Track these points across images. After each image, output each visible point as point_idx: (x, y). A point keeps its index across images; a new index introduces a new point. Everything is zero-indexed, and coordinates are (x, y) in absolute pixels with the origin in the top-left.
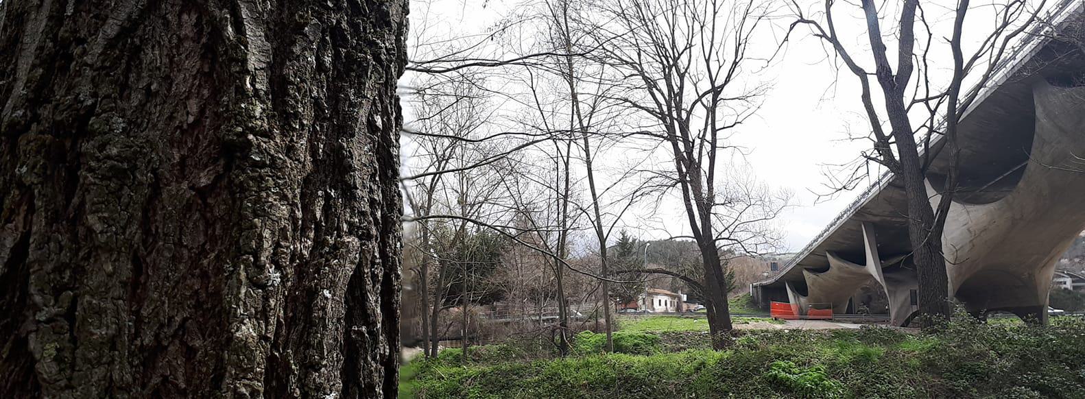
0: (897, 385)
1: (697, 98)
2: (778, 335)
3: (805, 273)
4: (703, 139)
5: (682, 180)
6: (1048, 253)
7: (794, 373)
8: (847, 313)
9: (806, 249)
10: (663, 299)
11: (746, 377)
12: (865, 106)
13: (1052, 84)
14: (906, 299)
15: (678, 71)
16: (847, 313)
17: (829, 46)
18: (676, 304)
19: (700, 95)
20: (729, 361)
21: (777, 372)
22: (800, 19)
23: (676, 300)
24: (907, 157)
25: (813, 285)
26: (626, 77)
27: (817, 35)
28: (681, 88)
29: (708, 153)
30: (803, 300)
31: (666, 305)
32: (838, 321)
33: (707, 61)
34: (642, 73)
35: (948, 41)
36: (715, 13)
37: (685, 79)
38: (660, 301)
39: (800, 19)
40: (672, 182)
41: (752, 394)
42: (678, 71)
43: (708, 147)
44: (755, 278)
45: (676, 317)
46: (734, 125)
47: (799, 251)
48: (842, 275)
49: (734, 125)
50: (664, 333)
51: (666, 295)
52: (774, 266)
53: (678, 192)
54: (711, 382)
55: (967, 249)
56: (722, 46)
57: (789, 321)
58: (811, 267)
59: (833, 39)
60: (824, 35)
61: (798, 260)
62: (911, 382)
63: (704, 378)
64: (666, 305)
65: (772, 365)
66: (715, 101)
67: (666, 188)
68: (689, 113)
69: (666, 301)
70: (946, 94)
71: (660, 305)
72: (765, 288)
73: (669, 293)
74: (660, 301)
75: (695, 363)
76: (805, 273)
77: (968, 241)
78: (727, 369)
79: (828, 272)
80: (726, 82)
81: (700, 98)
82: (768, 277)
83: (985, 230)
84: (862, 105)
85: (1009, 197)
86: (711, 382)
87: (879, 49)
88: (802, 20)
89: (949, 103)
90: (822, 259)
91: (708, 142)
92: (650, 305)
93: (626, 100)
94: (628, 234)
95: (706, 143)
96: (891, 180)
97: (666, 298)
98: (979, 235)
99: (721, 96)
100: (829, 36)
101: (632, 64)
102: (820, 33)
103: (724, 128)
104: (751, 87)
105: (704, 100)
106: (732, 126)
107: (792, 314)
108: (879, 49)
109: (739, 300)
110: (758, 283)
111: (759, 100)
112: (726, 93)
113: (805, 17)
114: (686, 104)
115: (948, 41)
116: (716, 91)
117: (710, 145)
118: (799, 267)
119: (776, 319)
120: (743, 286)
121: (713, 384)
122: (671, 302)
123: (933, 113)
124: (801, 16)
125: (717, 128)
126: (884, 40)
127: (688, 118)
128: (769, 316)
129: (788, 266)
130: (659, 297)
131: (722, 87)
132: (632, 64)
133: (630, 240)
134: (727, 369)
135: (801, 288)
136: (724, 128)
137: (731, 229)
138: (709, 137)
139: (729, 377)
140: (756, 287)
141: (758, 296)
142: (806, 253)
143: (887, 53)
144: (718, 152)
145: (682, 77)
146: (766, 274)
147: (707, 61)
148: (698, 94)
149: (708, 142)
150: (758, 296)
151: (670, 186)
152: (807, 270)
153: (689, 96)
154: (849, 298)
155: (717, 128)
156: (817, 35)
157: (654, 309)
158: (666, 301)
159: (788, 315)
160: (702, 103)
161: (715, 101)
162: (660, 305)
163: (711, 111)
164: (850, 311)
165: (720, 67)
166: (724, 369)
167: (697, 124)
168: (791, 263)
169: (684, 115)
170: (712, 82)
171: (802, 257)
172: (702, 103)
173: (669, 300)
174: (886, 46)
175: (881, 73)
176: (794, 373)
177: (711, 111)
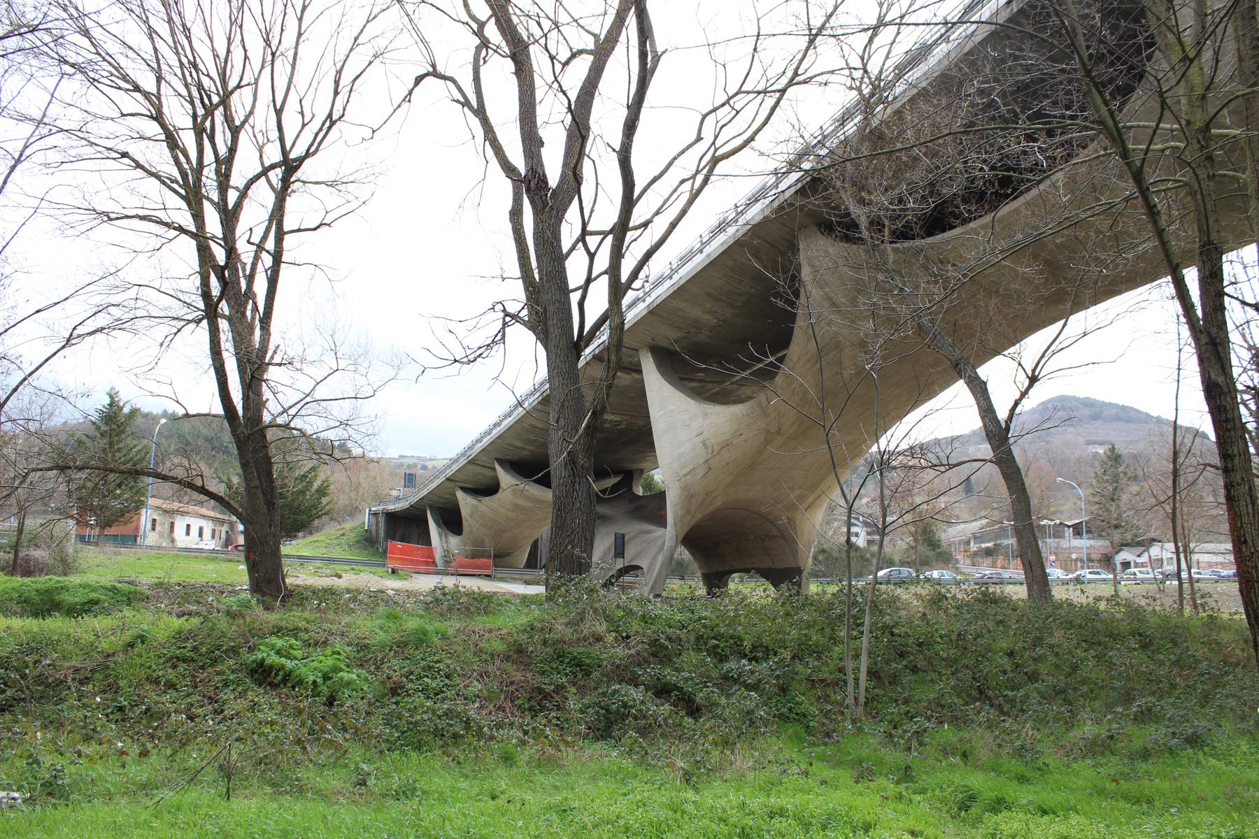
0: (457, 680)
1: (260, 169)
2: (377, 597)
3: (460, 495)
4: (260, 247)
5: (211, 313)
6: (812, 489)
7: (296, 658)
8: (525, 567)
9: (463, 454)
10: (196, 524)
11: (215, 661)
12: (513, 228)
13: (821, 233)
14: (609, 549)
15: (228, 119)
16: (525, 567)
17: (475, 122)
18: (224, 536)
19: (266, 165)
20: (191, 635)
21: (265, 655)
22: (431, 70)
23: (225, 528)
24: (555, 322)
25: (471, 516)
26: (123, 115)
27: (458, 101)
28: (232, 150)
29: (266, 271)
30: (454, 541)
31: (201, 535)
32: (502, 580)
33: (279, 113)
34: (158, 118)
35: (614, 150)
36: (300, 35)
37: (243, 136)
38: (188, 526)
39: (431, 70)
40: (195, 314)
41: (217, 688)
42: (228, 119)
43: (267, 260)
44: (380, 499)
45: (206, 558)
46: (318, 227)
47: (453, 455)
48: (520, 502)
49: (318, 227)
50: (159, 585)
51: (204, 516)
52: (410, 480)
53: (202, 333)
54: (150, 667)
55: (700, 472)
56: (312, 90)
57: (418, 576)
58: (470, 486)
59: (480, 112)
60: (466, 103)
61: (449, 473)
62: (482, 676)
63: (138, 661)
64: (201, 535)
65: (261, 644)
66: (286, 181)
67: (183, 323)
68: (243, 194)
69: (201, 529)
70: (611, 232)
71: (188, 534)
72: (391, 517)
73: (212, 514)
74: (188, 526)
75: (127, 636)
76: (460, 495)
77: (702, 460)
78: (184, 648)
79: (498, 496)
80: (308, 154)
81: (265, 172)
82: (400, 499)
83: (726, 445)
84: (510, 226)
85: (762, 397)
86: (150, 667)
87: (532, 142)
88: (435, 74)
89: (612, 245)
90: (488, 473)
91: (267, 252)
92: (167, 530)
93: (125, 155)
94: (123, 397)
95: (264, 255)
96: (597, 351)
97: (203, 523)
98: (719, 453)
99: (299, 174)
100: (474, 104)
101: (146, 95)
102: (462, 100)
103: (299, 230)
104: (346, 171)
105: (271, 174)
106: (315, 229)
107: (434, 563)
108: (532, 142)
109: (343, 535)
110: (381, 508)
111: (363, 192)
112: (304, 172)
113: (440, 69)
114: (238, 178)
115: (614, 150)
116: (290, 166)
117: (271, 258)
118: (450, 484)
119: (393, 572)
120: (353, 511)
121: (154, 671)
122: (214, 531)
123: (592, 256)
124: (434, 66)
125: (286, 230)
126: (542, 132)
127: (239, 205)
128: (384, 566)
129: (432, 481)
130: (188, 520)
131: (301, 160)
132: (146, 95)
133: (126, 410)
134: (184, 648)
135: (452, 521)
136: (299, 230)
137: (293, 411)
138: (270, 244)
139: (184, 661)
140: (376, 514)
141: (377, 530)
142: (463, 461)
143: (544, 152)
144: (284, 271)
145: (235, 131)
146: (395, 493)
147: (279, 113)
148: (262, 164)
149: (267, 252)
150: (377, 530)
151: (189, 322)
152: (464, 489)
153: (244, 167)
154: (531, 541)
155: (286, 230)
156: (458, 101)
157: (173, 541)
158: (201, 529)
159: (429, 566)
160: (269, 181)
161: (286, 181)
162: (188, 534)
163: (282, 195)
164: (532, 563)
165: (304, 125)
166: (180, 648)
167: (254, 217)
168: (437, 477)
169: (232, 197)
170: (285, 153)
171: (455, 467)
172: (269, 181)
173: (208, 527)
174: (544, 140)
175: (530, 181)
176: (296, 658)
177: (282, 195)
